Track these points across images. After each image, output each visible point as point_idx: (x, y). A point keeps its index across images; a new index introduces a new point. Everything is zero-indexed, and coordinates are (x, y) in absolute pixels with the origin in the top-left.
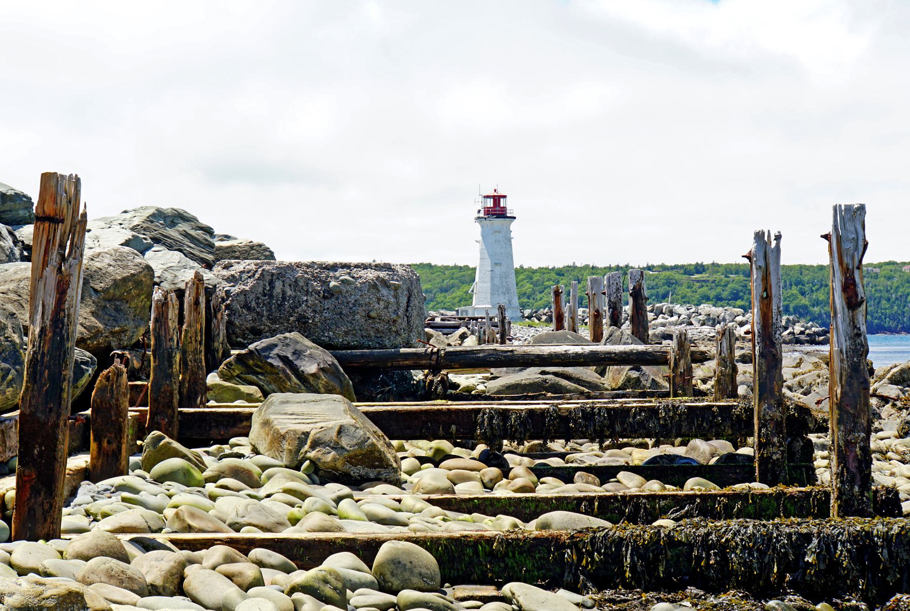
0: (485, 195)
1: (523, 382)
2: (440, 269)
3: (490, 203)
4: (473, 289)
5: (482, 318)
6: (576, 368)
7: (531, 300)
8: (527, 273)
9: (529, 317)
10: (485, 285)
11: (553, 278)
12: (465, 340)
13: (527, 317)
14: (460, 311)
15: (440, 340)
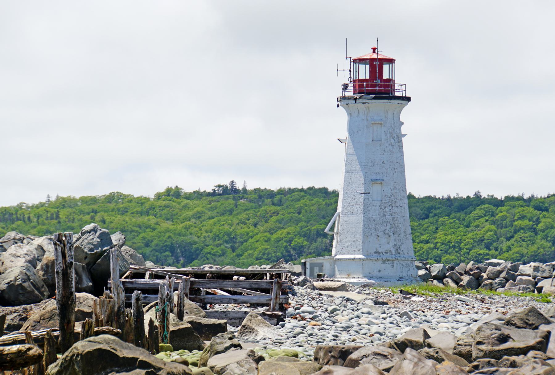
3: (364, 72)
9: (440, 278)
10: (353, 218)
11: (529, 215)
13: (436, 278)
14: (308, 266)
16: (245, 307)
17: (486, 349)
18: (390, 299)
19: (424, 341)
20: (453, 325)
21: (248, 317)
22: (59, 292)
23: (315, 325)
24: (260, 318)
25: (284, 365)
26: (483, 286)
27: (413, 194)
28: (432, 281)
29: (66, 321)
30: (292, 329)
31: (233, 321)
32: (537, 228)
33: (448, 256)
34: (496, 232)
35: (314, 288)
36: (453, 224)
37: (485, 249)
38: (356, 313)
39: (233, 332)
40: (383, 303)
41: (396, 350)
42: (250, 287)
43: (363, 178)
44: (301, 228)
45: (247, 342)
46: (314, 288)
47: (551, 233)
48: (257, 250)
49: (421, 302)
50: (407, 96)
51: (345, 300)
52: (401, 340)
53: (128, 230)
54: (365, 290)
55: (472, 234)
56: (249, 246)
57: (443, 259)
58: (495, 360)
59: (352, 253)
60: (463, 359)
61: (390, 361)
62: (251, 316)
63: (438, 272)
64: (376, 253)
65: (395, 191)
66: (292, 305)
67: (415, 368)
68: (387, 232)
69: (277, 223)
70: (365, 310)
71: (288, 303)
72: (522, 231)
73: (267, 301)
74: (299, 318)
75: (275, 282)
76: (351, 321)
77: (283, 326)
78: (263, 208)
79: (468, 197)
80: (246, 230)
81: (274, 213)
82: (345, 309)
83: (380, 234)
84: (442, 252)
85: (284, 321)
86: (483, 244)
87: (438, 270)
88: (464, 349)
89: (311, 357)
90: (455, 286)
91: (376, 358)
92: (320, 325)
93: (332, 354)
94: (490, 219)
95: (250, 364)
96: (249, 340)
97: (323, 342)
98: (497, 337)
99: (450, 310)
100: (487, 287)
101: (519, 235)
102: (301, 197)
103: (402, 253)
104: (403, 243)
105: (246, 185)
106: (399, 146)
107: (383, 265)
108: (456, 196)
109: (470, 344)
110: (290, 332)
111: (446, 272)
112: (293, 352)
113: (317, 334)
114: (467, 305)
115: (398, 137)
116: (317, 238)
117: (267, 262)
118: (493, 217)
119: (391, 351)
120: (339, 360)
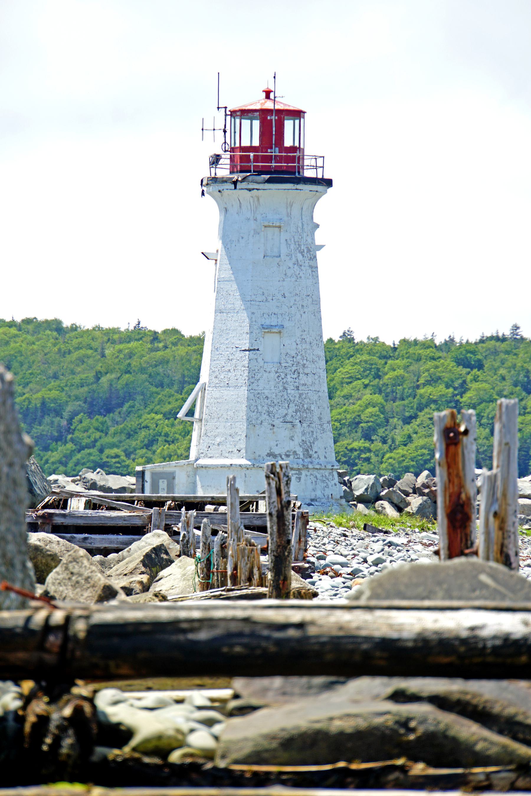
0: (233, 106)
1: (337, 726)
2: (86, 340)
4: (194, 405)
5: (219, 502)
6: (505, 683)
7: (377, 445)
8: (365, 357)
10: (229, 394)
11: (446, 376)
12: (162, 573)
13: (361, 500)
14: (148, 477)
15: (80, 575)
22: (272, 540)
28: (355, 506)
29: (282, 578)
32: (461, 400)
37: (362, 441)
47: (488, 411)
50: (326, 177)
53: (363, 462)
59: (227, 455)
63: (366, 489)
64: (269, 455)
68: (289, 418)
72: (433, 406)
75: (298, 516)
83: (277, 422)
86: (360, 430)
87: (365, 487)
94: (372, 383)
101: (426, 413)
104: (317, 439)
106: (311, 267)
111: (379, 489)
115: (309, 251)
116: (43, 417)
118: (377, 380)
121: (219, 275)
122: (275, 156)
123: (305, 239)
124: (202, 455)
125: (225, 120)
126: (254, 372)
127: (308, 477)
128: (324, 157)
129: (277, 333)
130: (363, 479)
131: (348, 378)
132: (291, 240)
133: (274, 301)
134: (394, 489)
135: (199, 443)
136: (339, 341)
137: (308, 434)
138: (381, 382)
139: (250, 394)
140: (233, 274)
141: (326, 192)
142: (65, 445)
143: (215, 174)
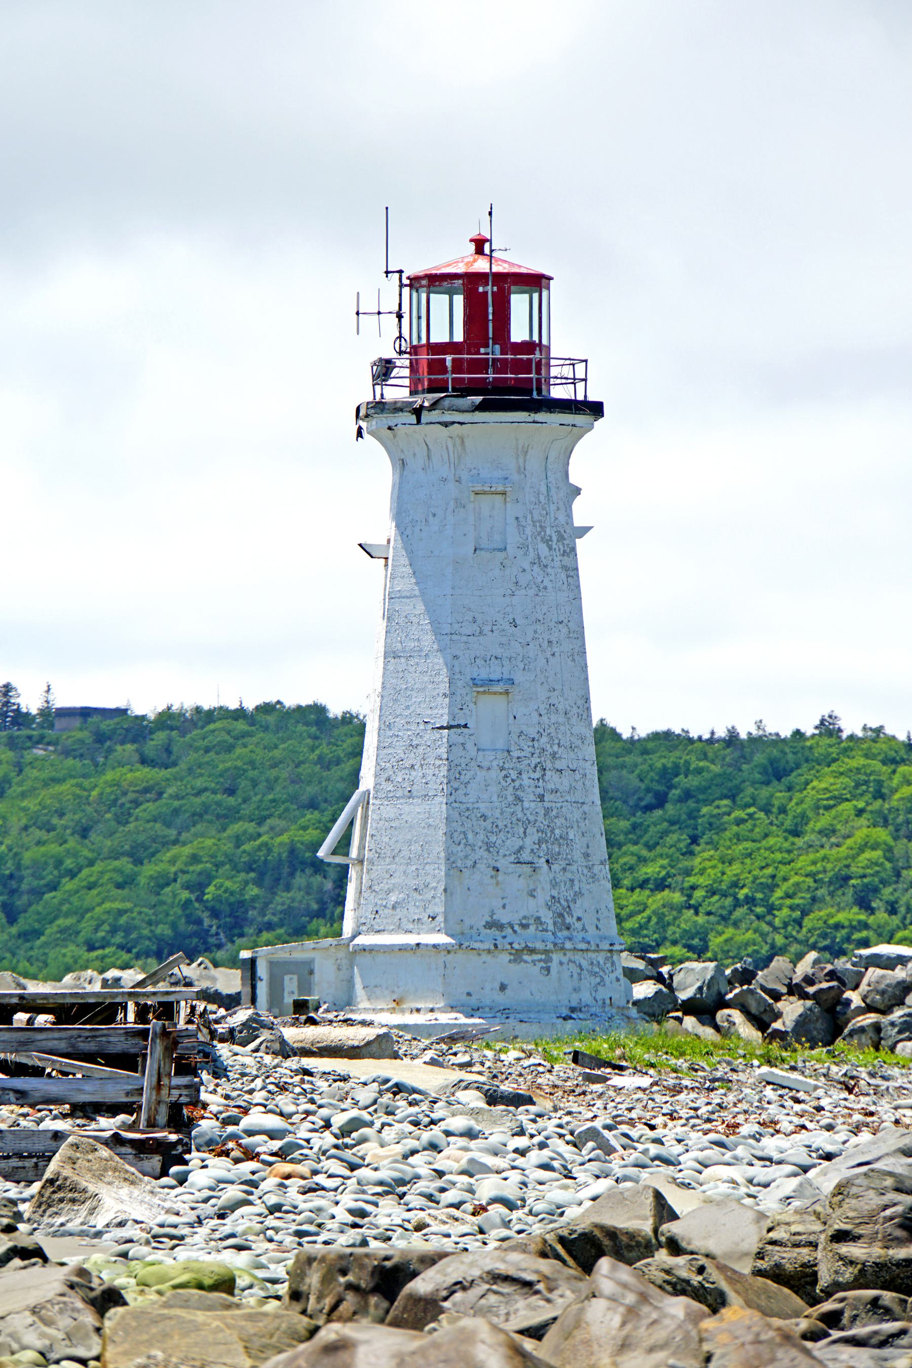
8: (859, 761)
10: (414, 810)
13: (690, 1007)
14: (262, 970)
16: (55, 1118)
17: (864, 1257)
18: (539, 1081)
19: (656, 1231)
20: (751, 1171)
21: (63, 1150)
23: (288, 1177)
24: (105, 1152)
25: (191, 1321)
26: (851, 1034)
27: (612, 723)
28: (680, 1020)
30: (211, 1189)
31: (14, 1162)
33: (730, 932)
34: (890, 849)
35: (285, 1051)
36: (749, 825)
37: (856, 909)
38: (426, 1136)
39: (14, 1202)
40: (518, 1100)
41: (564, 1262)
42: (70, 1050)
43: (444, 677)
44: (238, 841)
45: (63, 1235)
46: (285, 1051)
48: (88, 915)
49: (644, 1090)
50: (591, 398)
51: (388, 1090)
52: (580, 1229)
54: (455, 1054)
55: (812, 856)
56: (61, 903)
57: (715, 941)
58: (894, 1294)
59: (410, 926)
60: (786, 1291)
61: (542, 1303)
62: (75, 1146)
63: (700, 989)
64: (489, 925)
65: (554, 718)
66: (213, 1108)
67: (629, 1327)
68: (526, 856)
69: (158, 826)
70: (458, 1123)
71: (197, 1103)
73: (127, 1094)
74: (236, 1154)
75: (155, 1033)
76: (411, 1160)
77: (182, 1180)
78: (109, 776)
79: (798, 733)
80: (54, 849)
81: (146, 790)
82: (389, 1119)
83: (502, 863)
84: (712, 918)
85: (186, 1163)
87: (699, 984)
88: (790, 1258)
89: (277, 1286)
90: (756, 1035)
91: (496, 1293)
92: (308, 1175)
93: (350, 1278)
94: (869, 808)
95: (75, 1315)
96: (69, 1226)
97: (317, 1234)
98: (903, 1216)
99: (740, 1119)
100: (864, 1038)
102: (236, 738)
103: (578, 925)
105: (51, 698)
106: (565, 568)
107: (516, 969)
108: (755, 732)
109: (812, 1238)
110: (206, 1200)
111: (724, 987)
112: (216, 1269)
113: (296, 1207)
114: (797, 1101)
115: (561, 538)
116: (292, 874)
117: (126, 957)
118: (880, 801)
119: (546, 1266)
120: (373, 1300)
121: (392, 587)
122: (493, 359)
123: (552, 515)
124: (364, 928)
125: (400, 295)
126: (459, 768)
127: (565, 966)
128: (586, 361)
129: (501, 693)
130: (693, 970)
131: (827, 799)
132: (526, 517)
133: (496, 633)
134: (752, 987)
135: (359, 904)
136: (814, 735)
137: (562, 885)
138: (887, 806)
139: (451, 812)
140: (417, 583)
141: (591, 427)
142: (332, 925)
143: (382, 395)
